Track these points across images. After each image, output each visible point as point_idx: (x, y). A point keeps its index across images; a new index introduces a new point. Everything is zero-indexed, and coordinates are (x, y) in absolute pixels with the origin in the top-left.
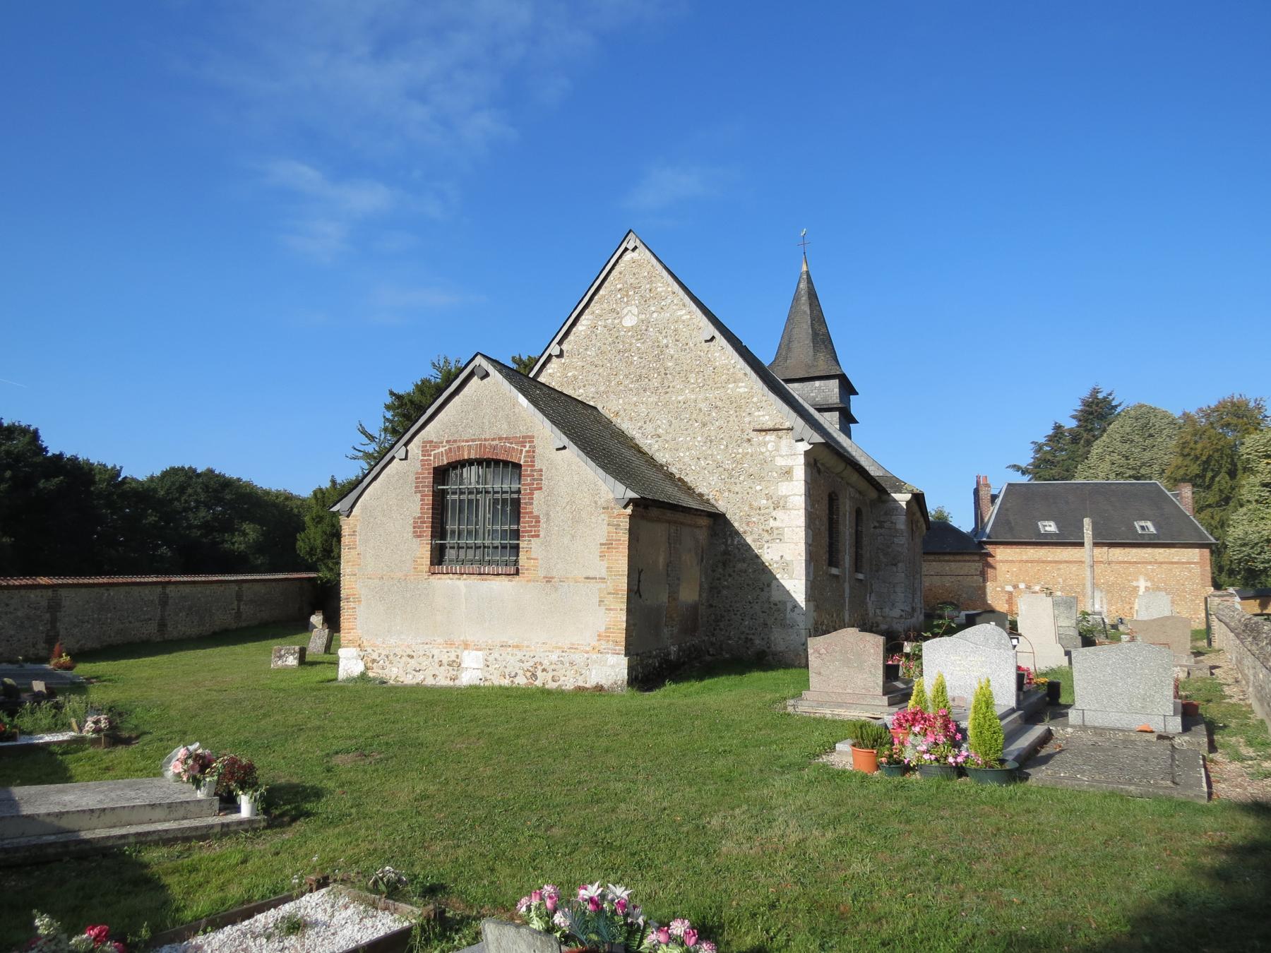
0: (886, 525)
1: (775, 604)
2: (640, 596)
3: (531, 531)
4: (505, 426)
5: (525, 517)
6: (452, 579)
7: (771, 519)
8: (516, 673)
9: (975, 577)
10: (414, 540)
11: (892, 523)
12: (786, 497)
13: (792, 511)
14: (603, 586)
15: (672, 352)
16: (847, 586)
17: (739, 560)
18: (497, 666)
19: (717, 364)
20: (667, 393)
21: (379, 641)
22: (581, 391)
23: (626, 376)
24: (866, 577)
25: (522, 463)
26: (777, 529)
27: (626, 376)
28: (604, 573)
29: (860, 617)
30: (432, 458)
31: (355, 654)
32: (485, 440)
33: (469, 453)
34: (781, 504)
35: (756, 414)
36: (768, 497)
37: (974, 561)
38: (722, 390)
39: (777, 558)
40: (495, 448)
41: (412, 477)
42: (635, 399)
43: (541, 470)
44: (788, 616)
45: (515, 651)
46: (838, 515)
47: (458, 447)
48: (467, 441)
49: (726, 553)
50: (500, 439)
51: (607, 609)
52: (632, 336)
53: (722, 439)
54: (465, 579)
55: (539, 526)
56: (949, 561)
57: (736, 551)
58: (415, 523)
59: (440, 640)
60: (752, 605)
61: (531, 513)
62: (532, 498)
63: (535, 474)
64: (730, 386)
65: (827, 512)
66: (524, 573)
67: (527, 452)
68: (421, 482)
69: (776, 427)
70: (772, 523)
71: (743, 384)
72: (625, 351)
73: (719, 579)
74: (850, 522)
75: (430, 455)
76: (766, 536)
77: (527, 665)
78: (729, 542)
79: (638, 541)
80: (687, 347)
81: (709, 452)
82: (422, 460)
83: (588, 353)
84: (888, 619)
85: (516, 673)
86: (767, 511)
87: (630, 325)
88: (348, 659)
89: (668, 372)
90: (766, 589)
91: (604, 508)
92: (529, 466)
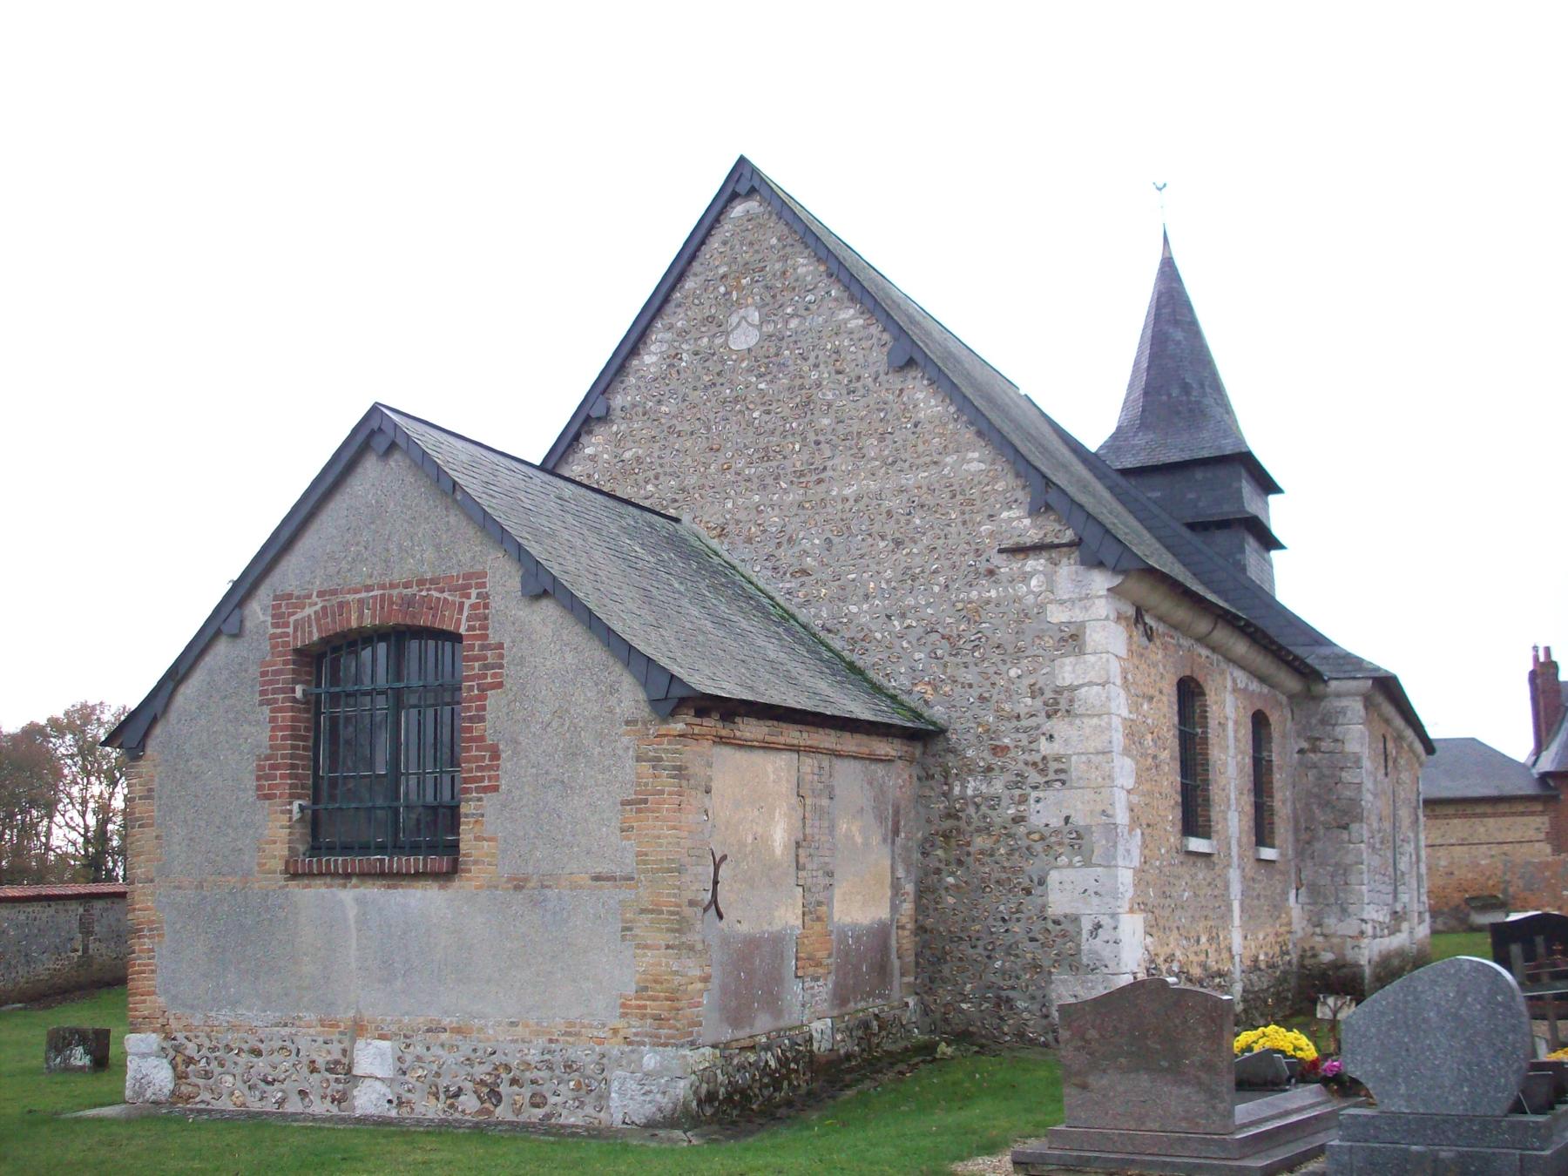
0: (1324, 745)
1: (1056, 922)
2: (721, 916)
3: (482, 779)
4: (430, 554)
5: (468, 749)
6: (331, 886)
7: (1043, 739)
8: (460, 1089)
9: (1537, 845)
10: (259, 803)
11: (1337, 740)
12: (1073, 688)
13: (1086, 720)
14: (626, 894)
15: (830, 396)
16: (1234, 875)
17: (978, 830)
18: (420, 1072)
19: (922, 415)
20: (820, 481)
21: (197, 1020)
22: (650, 487)
23: (739, 451)
24: (1281, 854)
25: (462, 631)
26: (1058, 759)
27: (739, 451)
28: (629, 864)
29: (1271, 939)
30: (290, 630)
31: (155, 1047)
32: (392, 586)
33: (361, 616)
34: (1063, 705)
35: (1005, 515)
36: (1035, 692)
37: (1533, 813)
38: (934, 470)
39: (1056, 822)
40: (409, 602)
41: (254, 670)
42: (757, 498)
43: (500, 646)
44: (1085, 947)
45: (457, 1039)
46: (1205, 726)
47: (341, 605)
48: (356, 591)
49: (952, 815)
50: (421, 582)
51: (638, 946)
52: (750, 370)
53: (935, 572)
54: (355, 886)
55: (498, 767)
56: (1485, 815)
57: (971, 810)
58: (260, 768)
59: (309, 1016)
60: (1010, 925)
61: (482, 738)
62: (483, 708)
63: (489, 653)
64: (948, 460)
65: (1176, 719)
66: (469, 871)
67: (473, 607)
68: (271, 682)
69: (1048, 540)
70: (1044, 747)
71: (976, 455)
72: (736, 400)
73: (938, 871)
74: (1237, 740)
75: (286, 625)
76: (1034, 777)
77: (480, 1072)
78: (957, 790)
79: (708, 792)
80: (859, 385)
81: (910, 601)
82: (273, 636)
83: (664, 409)
84: (1335, 940)
85: (460, 1089)
86: (1033, 722)
87: (745, 347)
88: (144, 1056)
89: (822, 438)
90: (1037, 891)
91: (627, 723)
92: (476, 637)
